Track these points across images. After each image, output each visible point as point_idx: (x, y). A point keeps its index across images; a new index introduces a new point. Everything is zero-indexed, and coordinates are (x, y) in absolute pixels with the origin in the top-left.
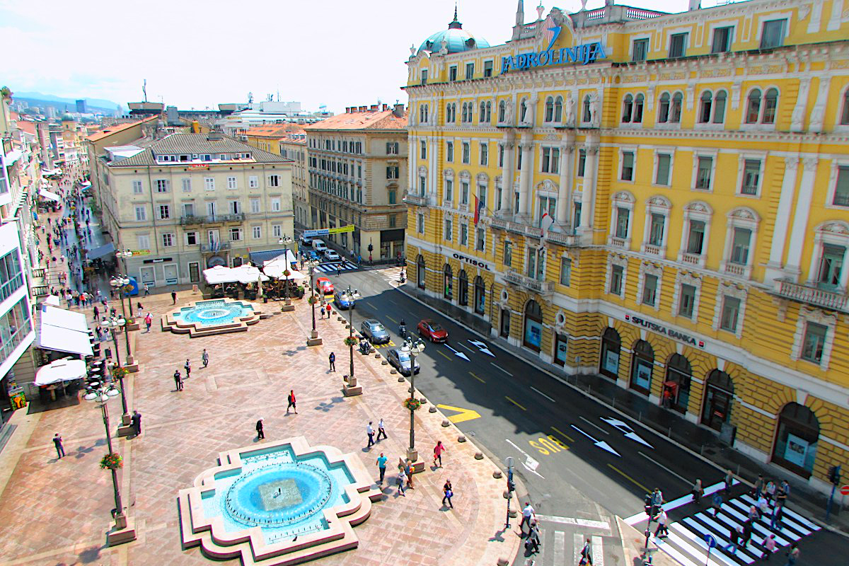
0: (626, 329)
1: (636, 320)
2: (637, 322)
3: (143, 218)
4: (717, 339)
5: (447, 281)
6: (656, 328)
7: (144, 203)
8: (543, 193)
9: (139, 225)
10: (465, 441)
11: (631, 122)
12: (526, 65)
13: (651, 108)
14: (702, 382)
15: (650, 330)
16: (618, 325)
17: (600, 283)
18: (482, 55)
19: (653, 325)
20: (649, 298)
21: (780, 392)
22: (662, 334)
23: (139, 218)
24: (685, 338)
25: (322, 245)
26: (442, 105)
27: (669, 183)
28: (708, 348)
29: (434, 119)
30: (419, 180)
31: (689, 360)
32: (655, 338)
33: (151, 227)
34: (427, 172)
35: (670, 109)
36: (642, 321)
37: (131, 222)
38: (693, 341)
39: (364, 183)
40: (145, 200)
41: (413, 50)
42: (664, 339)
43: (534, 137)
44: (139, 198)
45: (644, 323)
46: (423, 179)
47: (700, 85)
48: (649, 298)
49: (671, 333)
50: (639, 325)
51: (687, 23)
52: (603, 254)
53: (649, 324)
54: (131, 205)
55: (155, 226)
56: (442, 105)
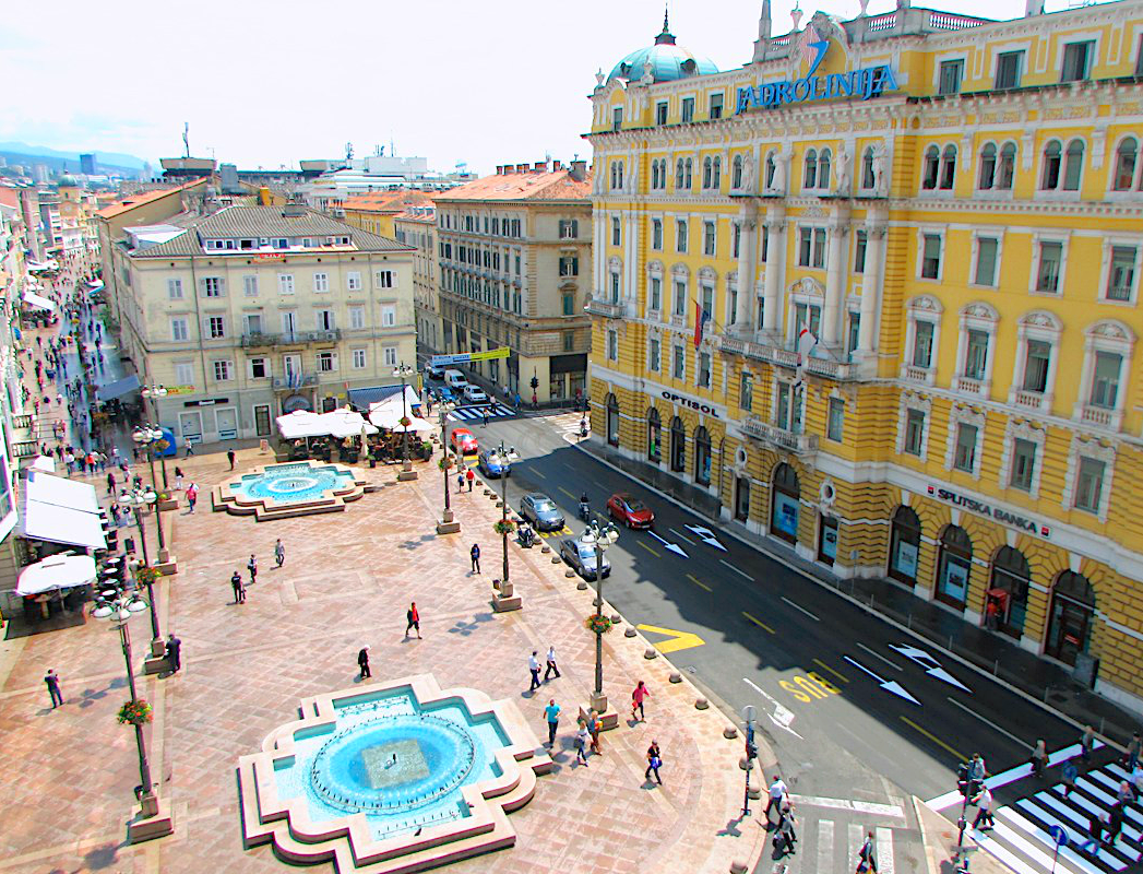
0: (929, 508)
1: (945, 495)
2: (946, 497)
3: (184, 337)
4: (1069, 523)
5: (653, 434)
6: (976, 506)
7: (185, 313)
8: (801, 299)
9: (177, 348)
10: (680, 681)
11: (937, 189)
12: (775, 100)
13: (968, 167)
14: (1045, 590)
15: (966, 509)
16: (917, 501)
17: (889, 438)
18: (707, 85)
19: (970, 502)
20: (964, 459)
21: (1053, 556)
22: (985, 516)
23: (177, 337)
24: (1020, 522)
25: (460, 379)
26: (646, 163)
27: (996, 283)
28: (1056, 538)
29: (632, 183)
30: (610, 278)
31: (1026, 556)
32: (974, 522)
33: (195, 351)
34: (622, 266)
35: (996, 168)
36: (953, 496)
37: (164, 343)
38: (1032, 526)
39: (524, 283)
40: (186, 309)
41: (600, 77)
42: (987, 524)
43: (787, 211)
44: (178, 306)
45: (957, 499)
46: (615, 276)
47: (1043, 131)
48: (964, 459)
49: (999, 514)
50: (949, 502)
51: (1023, 35)
52: (893, 393)
53: (964, 501)
54: (165, 316)
55: (201, 349)
56: (646, 163)
